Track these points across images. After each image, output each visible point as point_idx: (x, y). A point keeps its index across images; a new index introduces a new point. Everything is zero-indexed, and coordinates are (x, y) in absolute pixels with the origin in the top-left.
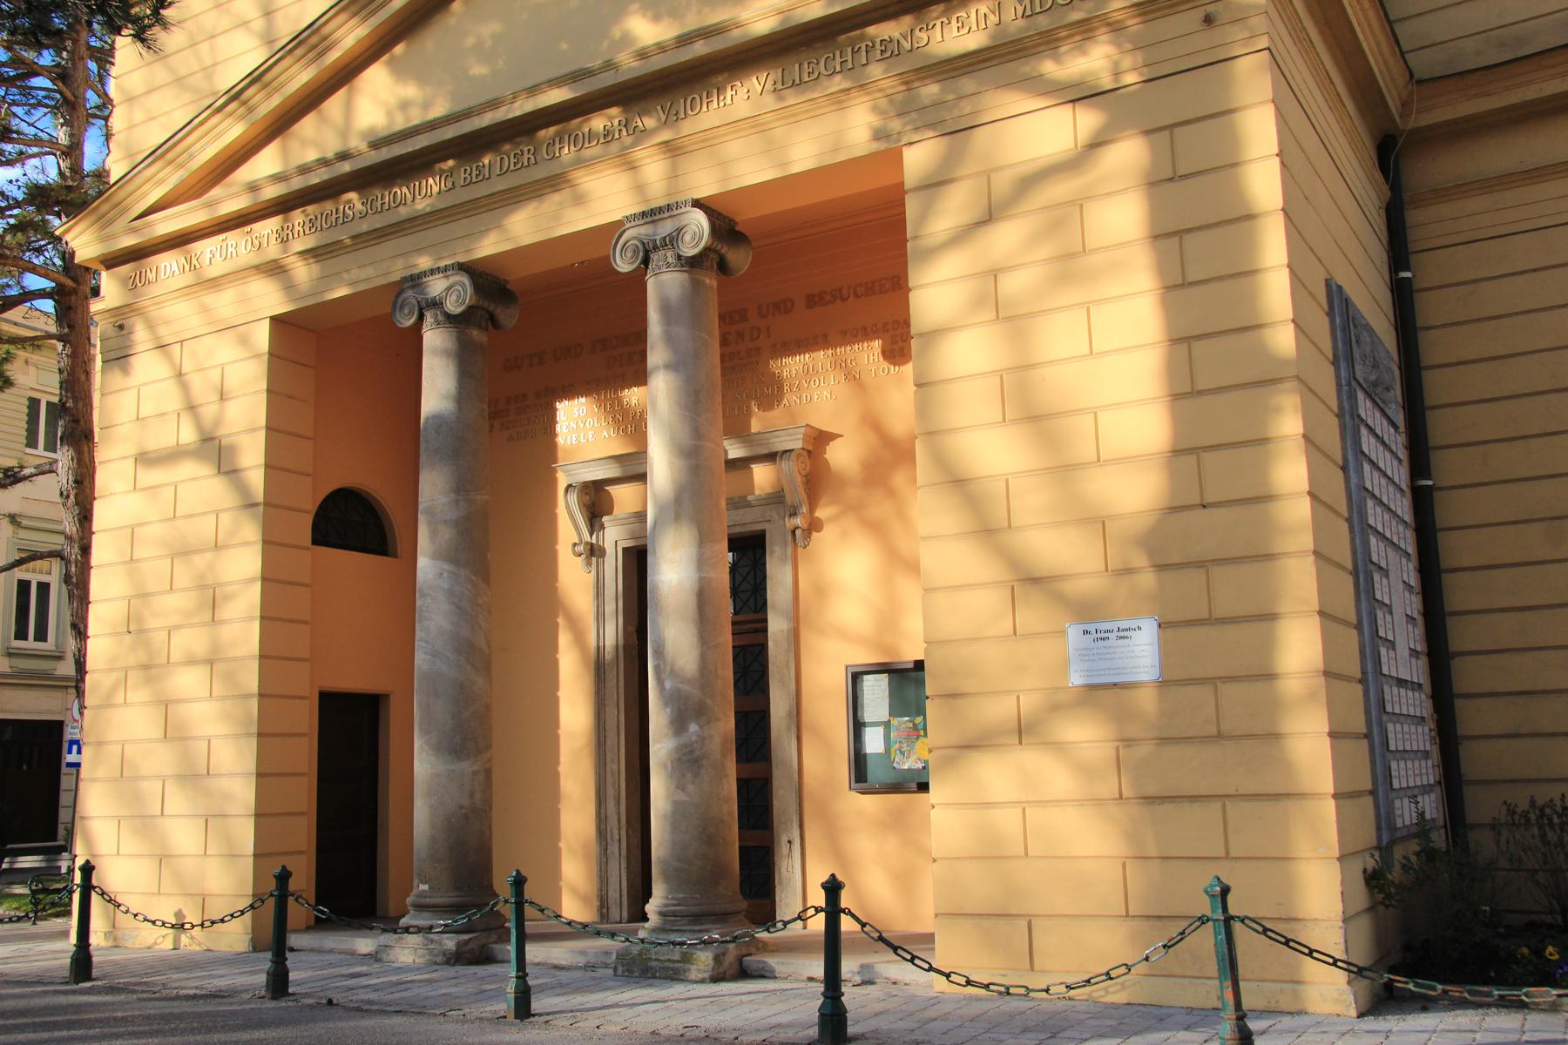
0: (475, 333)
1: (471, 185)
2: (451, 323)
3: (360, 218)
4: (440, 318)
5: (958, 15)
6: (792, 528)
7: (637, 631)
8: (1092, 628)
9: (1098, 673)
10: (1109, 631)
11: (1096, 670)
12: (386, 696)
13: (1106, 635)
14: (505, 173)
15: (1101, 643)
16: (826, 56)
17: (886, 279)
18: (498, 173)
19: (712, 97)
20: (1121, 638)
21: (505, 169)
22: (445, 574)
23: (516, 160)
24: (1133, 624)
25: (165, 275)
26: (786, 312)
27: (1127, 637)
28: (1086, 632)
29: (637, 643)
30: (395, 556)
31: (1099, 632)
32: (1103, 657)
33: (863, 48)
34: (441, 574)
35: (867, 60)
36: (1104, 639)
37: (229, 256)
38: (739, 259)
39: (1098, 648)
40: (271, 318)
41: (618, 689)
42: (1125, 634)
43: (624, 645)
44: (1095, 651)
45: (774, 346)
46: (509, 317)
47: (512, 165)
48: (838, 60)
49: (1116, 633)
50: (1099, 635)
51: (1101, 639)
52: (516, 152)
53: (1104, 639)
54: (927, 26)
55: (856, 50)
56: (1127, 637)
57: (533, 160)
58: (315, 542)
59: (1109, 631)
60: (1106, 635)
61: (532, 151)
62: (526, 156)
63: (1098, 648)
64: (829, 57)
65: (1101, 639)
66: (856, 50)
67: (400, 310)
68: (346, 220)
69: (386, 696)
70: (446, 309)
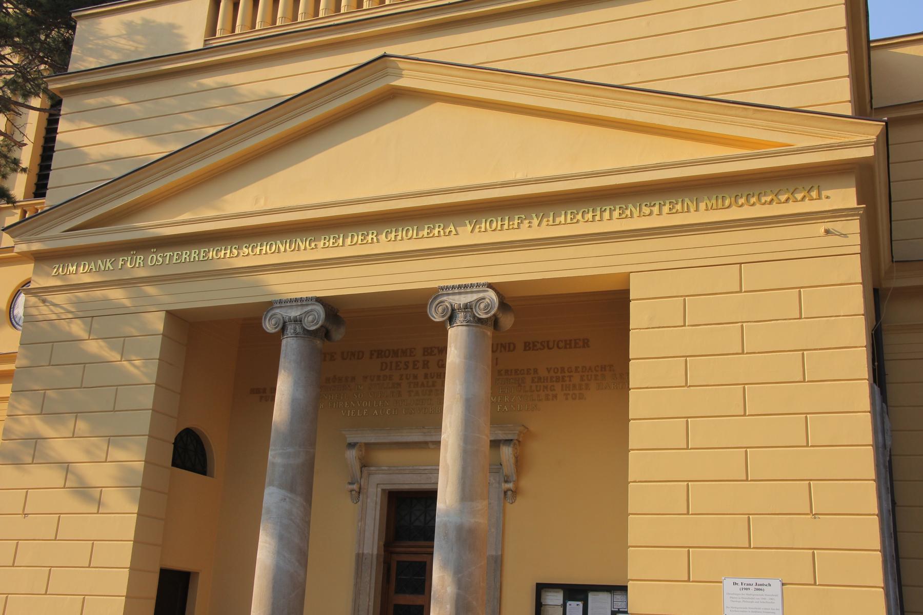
0: (318, 342)
1: (358, 246)
2: (305, 335)
3: (243, 256)
4: (298, 330)
5: (724, 195)
6: (506, 490)
7: (384, 545)
8: (739, 581)
9: (742, 610)
10: (750, 585)
11: (742, 608)
12: (197, 574)
13: (748, 587)
14: (353, 245)
15: (745, 592)
16: (387, 230)
17: (435, 347)
18: (81, 272)
19: (263, 247)
20: (758, 589)
21: (154, 264)
22: (288, 500)
23: (177, 258)
24: (766, 582)
25: (55, 273)
26: (358, 358)
27: (761, 590)
28: (735, 584)
29: (383, 553)
30: (212, 476)
31: (743, 585)
32: (745, 600)
33: (168, 256)
34: (285, 499)
35: (169, 262)
36: (746, 589)
37: (137, 265)
38: (507, 321)
39: (742, 594)
40: (167, 312)
41: (370, 584)
42: (760, 587)
43: (377, 554)
44: (741, 596)
45: (366, 377)
46: (338, 335)
47: (202, 257)
48: (394, 234)
49: (754, 586)
50: (743, 586)
51: (745, 589)
52: (124, 258)
53: (746, 589)
54: (650, 204)
55: (603, 210)
56: (761, 590)
57: (375, 240)
58: (175, 464)
59: (750, 585)
60: (748, 587)
61: (197, 253)
62: (370, 236)
63: (742, 594)
64: (585, 211)
65: (745, 589)
66: (603, 210)
67: (269, 320)
68: (157, 263)
69: (197, 574)
70: (304, 325)
